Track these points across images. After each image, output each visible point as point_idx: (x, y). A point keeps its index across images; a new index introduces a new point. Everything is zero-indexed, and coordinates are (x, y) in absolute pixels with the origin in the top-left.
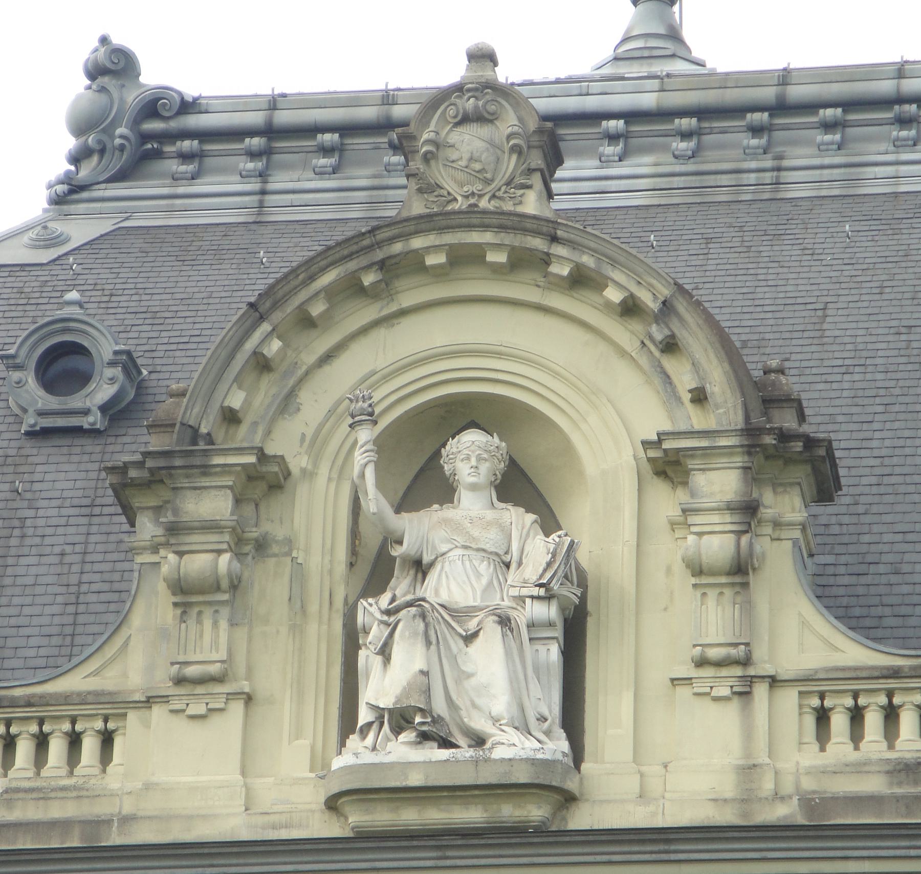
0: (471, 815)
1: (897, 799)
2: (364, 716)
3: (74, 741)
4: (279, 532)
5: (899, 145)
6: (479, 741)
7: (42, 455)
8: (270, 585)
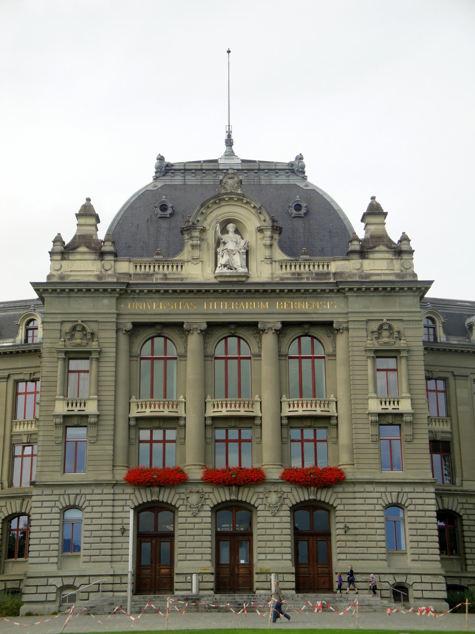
0: (235, 279)
1: (293, 278)
2: (219, 265)
3: (177, 266)
4: (205, 238)
5: (276, 176)
6: (236, 269)
7: (161, 220)
8: (204, 245)
